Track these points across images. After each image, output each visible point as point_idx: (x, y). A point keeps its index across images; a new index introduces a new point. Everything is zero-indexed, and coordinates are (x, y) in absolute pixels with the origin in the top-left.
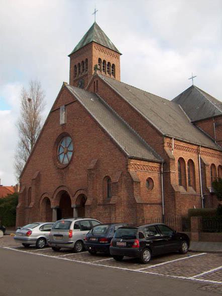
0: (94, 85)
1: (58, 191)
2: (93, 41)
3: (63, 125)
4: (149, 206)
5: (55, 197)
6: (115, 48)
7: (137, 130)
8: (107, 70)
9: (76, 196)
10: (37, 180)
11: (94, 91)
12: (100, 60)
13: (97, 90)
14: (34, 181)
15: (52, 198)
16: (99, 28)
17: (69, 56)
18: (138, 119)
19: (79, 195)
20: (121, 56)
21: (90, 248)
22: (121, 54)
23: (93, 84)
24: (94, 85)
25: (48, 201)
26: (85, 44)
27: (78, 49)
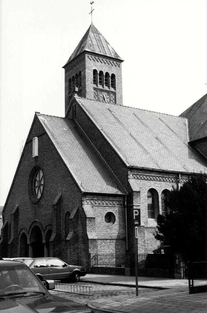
0: (73, 110)
1: (33, 226)
2: (85, 51)
3: (37, 157)
4: (108, 241)
5: (30, 233)
6: (116, 53)
7: (108, 161)
8: (105, 81)
9: (46, 232)
10: (16, 214)
11: (73, 117)
12: (95, 71)
13: (75, 116)
14: (13, 215)
15: (28, 233)
16: (96, 32)
17: (63, 67)
18: (108, 149)
19: (48, 231)
20: (122, 63)
21: (188, 262)
22: (123, 61)
23: (72, 109)
24: (73, 110)
25: (24, 236)
26: (78, 54)
27: (72, 58)
